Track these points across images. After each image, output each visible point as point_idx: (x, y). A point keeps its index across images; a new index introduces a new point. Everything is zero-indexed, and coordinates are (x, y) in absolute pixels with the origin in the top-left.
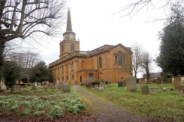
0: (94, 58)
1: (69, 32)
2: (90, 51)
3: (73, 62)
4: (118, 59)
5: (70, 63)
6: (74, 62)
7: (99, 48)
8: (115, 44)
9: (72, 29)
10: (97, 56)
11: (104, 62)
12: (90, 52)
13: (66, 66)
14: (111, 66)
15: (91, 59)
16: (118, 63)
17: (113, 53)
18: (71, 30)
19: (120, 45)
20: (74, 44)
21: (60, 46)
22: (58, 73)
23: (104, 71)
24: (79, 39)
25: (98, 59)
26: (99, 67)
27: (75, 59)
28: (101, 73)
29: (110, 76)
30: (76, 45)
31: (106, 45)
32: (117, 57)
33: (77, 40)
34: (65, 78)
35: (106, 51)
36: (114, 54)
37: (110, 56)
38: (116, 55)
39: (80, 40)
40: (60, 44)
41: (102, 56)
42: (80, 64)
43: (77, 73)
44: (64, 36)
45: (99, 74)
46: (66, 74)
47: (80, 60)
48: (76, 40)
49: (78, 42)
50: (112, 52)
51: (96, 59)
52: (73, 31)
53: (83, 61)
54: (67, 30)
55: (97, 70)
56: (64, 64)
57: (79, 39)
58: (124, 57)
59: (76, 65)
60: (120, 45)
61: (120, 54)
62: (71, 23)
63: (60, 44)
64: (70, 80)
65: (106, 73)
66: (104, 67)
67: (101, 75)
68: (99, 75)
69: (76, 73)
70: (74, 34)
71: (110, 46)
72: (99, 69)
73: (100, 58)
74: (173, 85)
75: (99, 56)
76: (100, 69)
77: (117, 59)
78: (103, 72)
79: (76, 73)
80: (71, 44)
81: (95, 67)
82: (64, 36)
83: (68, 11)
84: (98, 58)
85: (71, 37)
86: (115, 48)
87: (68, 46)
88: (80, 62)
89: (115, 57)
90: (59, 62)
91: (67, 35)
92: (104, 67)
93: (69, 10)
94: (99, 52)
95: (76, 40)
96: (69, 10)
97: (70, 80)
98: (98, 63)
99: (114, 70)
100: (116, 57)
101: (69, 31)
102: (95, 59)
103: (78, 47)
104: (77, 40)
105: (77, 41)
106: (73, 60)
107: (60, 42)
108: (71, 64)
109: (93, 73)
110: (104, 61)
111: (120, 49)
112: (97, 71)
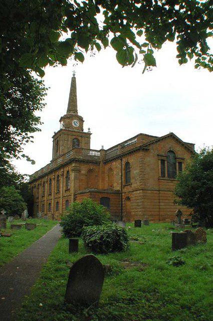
0: (114, 163)
1: (72, 115)
2: (106, 148)
3: (68, 171)
4: (168, 167)
5: (63, 175)
6: (71, 172)
7: (126, 142)
8: (160, 134)
9: (78, 109)
10: (121, 160)
11: (135, 172)
12: (106, 151)
13: (56, 179)
14: (152, 183)
15: (107, 167)
16: (166, 175)
17: (156, 153)
18: (76, 111)
19: (172, 136)
20: (80, 138)
21: (53, 141)
22: (43, 194)
23: (135, 192)
24: (89, 129)
25: (123, 166)
26: (124, 184)
27: (73, 165)
28: (128, 199)
29: (148, 207)
30: (83, 141)
31: (141, 134)
32: (166, 162)
33: (86, 130)
34: (53, 205)
35: (140, 147)
36: (158, 155)
37: (151, 160)
38: (163, 158)
39: (91, 131)
40: (53, 138)
41: (132, 160)
42: (83, 177)
43: (75, 195)
44: (62, 122)
45: (124, 200)
46: (56, 196)
47: (84, 169)
48: (84, 131)
49: (88, 135)
50: (154, 151)
51: (119, 166)
52: (80, 114)
53: (90, 171)
54: (69, 110)
55: (118, 191)
56: (52, 176)
57: (89, 129)
58: (180, 163)
59: (74, 179)
60: (171, 136)
61: (171, 155)
62: (76, 99)
63: (53, 138)
64: (61, 210)
65: (140, 198)
66: (134, 186)
67: (128, 203)
68: (124, 203)
69: (72, 195)
70: (81, 120)
71: (148, 136)
72: (125, 190)
73: (127, 163)
74: (68, 148)
75: (124, 160)
76: (125, 189)
77: (164, 167)
78: (133, 196)
79: (72, 197)
80: (74, 137)
81: (115, 185)
82: (62, 122)
83: (72, 78)
84: (124, 163)
85: (75, 123)
86: (162, 144)
87: (68, 141)
88: (83, 172)
89: (160, 161)
90: (51, 167)
91: (67, 121)
92: (134, 186)
93: (74, 75)
94: (125, 150)
95: (84, 131)
96: (74, 75)
97: (61, 210)
98: (122, 175)
99: (158, 192)
100: (163, 162)
101: (71, 113)
102: (116, 165)
103: (88, 143)
104: (86, 130)
105: (85, 133)
106: (70, 168)
107: (54, 134)
108: (65, 177)
109: (109, 198)
110: (135, 172)
111: (170, 144)
112: (118, 193)
